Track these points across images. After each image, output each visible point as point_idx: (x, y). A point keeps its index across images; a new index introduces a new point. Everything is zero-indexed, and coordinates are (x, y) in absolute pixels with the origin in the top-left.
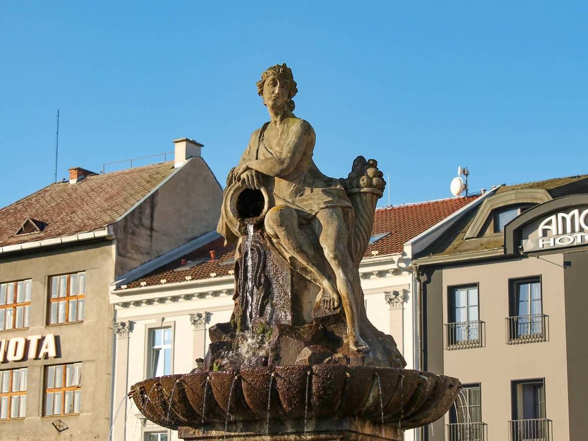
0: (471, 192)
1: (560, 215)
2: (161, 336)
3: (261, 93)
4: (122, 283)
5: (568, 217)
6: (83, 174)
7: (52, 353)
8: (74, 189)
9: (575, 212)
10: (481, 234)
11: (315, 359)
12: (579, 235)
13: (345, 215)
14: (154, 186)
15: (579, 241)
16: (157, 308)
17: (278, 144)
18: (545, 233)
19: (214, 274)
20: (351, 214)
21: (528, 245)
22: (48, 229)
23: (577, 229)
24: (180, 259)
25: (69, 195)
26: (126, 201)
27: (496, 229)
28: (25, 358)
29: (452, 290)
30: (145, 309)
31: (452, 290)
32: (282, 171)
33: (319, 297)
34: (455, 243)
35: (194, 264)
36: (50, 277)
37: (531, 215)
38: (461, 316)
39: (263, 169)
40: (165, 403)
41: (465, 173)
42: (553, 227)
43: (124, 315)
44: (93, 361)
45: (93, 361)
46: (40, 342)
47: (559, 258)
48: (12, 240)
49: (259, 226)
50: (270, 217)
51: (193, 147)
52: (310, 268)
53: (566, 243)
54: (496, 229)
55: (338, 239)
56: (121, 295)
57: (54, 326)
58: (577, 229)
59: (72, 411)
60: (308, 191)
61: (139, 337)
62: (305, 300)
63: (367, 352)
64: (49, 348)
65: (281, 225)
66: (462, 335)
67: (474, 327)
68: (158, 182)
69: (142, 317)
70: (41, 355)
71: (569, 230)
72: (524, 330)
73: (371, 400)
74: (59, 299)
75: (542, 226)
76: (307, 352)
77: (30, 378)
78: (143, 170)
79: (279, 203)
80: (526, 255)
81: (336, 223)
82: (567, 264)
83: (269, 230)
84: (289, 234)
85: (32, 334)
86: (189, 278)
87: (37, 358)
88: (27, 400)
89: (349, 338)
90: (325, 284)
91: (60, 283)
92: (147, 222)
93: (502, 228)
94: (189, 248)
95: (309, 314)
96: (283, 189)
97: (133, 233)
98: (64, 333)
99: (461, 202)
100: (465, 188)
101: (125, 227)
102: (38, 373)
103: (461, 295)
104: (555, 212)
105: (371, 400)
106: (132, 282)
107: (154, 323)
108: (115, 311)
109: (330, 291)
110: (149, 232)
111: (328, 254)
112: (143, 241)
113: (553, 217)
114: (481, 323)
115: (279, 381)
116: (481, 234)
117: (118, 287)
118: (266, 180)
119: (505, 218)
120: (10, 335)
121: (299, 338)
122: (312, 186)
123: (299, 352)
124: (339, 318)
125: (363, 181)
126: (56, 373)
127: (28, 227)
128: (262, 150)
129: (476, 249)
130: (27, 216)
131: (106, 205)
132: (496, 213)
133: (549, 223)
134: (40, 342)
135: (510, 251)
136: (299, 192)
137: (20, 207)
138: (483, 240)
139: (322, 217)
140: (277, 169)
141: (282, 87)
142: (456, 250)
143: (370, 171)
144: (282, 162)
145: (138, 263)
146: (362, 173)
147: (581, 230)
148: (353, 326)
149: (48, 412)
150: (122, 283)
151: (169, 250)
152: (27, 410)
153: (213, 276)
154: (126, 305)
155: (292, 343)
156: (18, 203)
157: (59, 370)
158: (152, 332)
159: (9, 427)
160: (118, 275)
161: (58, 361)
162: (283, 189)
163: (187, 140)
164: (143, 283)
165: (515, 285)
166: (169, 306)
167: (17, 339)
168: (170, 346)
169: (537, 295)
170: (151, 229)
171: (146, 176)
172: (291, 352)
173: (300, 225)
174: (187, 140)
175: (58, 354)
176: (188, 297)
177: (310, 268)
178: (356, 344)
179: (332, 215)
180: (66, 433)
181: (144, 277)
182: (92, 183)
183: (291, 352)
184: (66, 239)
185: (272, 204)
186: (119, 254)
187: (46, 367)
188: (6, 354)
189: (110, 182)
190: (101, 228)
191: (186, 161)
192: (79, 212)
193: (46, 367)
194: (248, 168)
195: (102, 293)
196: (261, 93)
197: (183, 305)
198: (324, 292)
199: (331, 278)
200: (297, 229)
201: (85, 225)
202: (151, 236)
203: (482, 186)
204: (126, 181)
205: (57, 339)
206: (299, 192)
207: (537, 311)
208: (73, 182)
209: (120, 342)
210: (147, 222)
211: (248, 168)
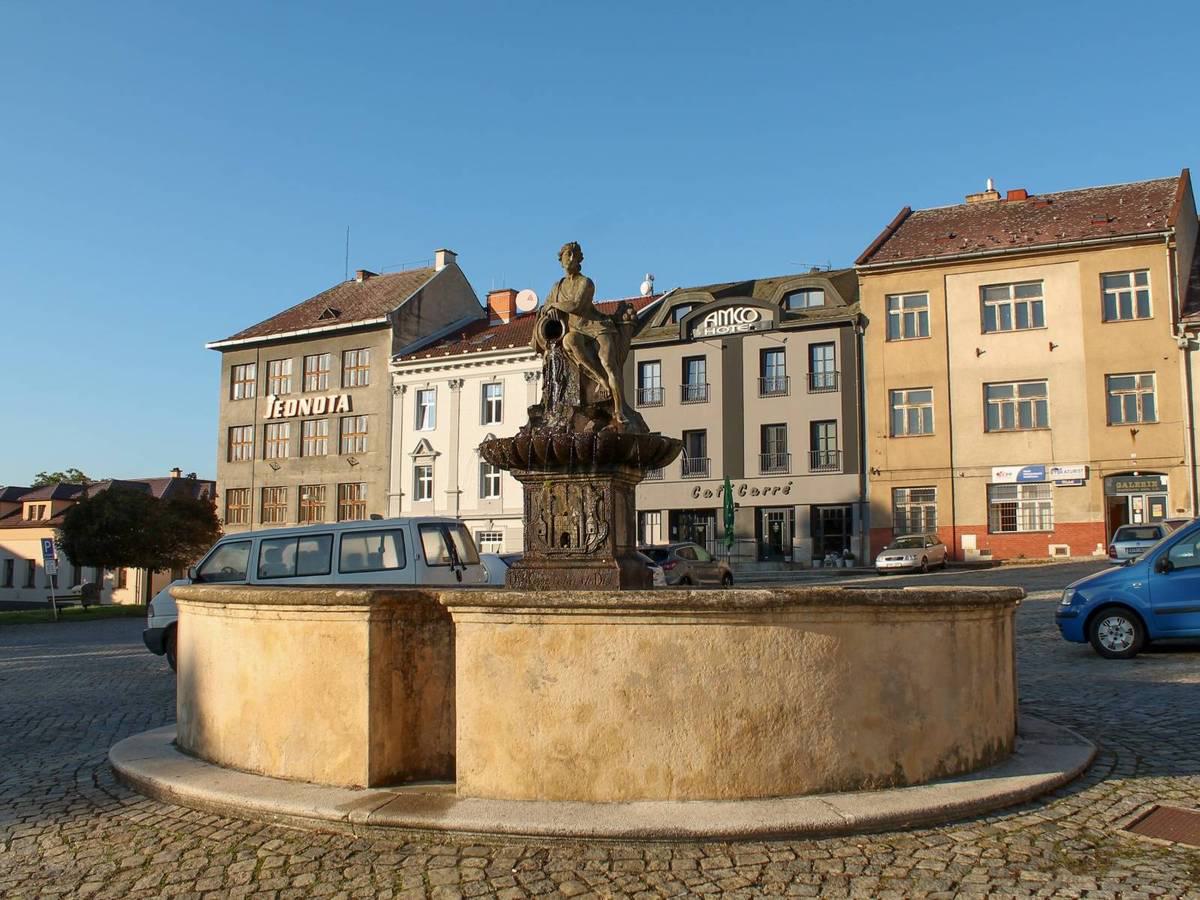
0: (655, 293)
1: (720, 312)
2: (426, 396)
3: (560, 260)
4: (398, 357)
5: (726, 313)
6: (366, 275)
7: (346, 408)
8: (361, 287)
9: (731, 309)
10: (663, 324)
11: (597, 428)
12: (733, 327)
13: (614, 337)
14: (421, 285)
15: (733, 331)
16: (424, 376)
17: (571, 293)
18: (709, 324)
19: (465, 351)
20: (617, 337)
21: (697, 333)
22: (342, 316)
23: (732, 322)
24: (439, 340)
25: (357, 291)
26: (400, 295)
27: (674, 321)
28: (326, 412)
29: (642, 365)
30: (414, 377)
31: (642, 365)
32: (575, 310)
33: (597, 390)
34: (644, 330)
35: (451, 343)
36: (344, 352)
37: (698, 312)
38: (648, 384)
39: (562, 308)
40: (504, 457)
41: (651, 279)
42: (715, 321)
43: (399, 380)
44: (376, 414)
45: (376, 414)
46: (337, 400)
47: (719, 343)
48: (314, 324)
49: (559, 344)
50: (567, 340)
51: (450, 255)
52: (592, 371)
53: (724, 332)
54: (674, 321)
55: (610, 354)
56: (396, 365)
57: (347, 388)
58: (732, 322)
59: (361, 449)
60: (590, 323)
61: (410, 398)
62: (589, 390)
63: (627, 424)
64: (344, 404)
65: (574, 344)
66: (648, 398)
67: (657, 391)
68: (424, 282)
69: (413, 382)
70: (338, 410)
71: (726, 323)
72: (694, 395)
73: (632, 453)
74: (350, 368)
75: (707, 319)
76: (591, 424)
77: (329, 427)
78: (412, 273)
79: (572, 330)
80: (695, 340)
81: (609, 344)
82: (724, 347)
83: (566, 347)
84: (580, 350)
85: (332, 394)
86: (447, 354)
87: (335, 412)
88: (328, 444)
89: (617, 413)
90: (602, 381)
91: (351, 356)
92: (416, 312)
93: (678, 320)
94: (445, 331)
95: (590, 398)
96: (575, 321)
97: (406, 320)
98: (354, 394)
99: (648, 300)
100: (651, 289)
101: (400, 314)
102: (336, 423)
103: (648, 368)
104: (717, 309)
105: (632, 453)
106: (405, 356)
107: (421, 386)
108: (393, 378)
109: (604, 386)
110: (416, 319)
111: (604, 362)
112: (413, 327)
113: (715, 313)
114: (662, 388)
115: (577, 442)
116: (663, 324)
117: (395, 360)
118: (563, 315)
119: (681, 313)
120: (314, 394)
121: (586, 415)
122: (593, 319)
123: (586, 424)
124: (610, 403)
125: (625, 317)
126: (349, 423)
127: (327, 315)
128: (560, 296)
129: (659, 335)
130: (326, 306)
131: (384, 299)
132: (673, 309)
133: (712, 317)
134: (337, 400)
135: (684, 337)
136: (584, 323)
137: (320, 299)
138: (665, 328)
139: (600, 340)
140: (572, 309)
141: (574, 257)
142: (644, 336)
143: (629, 311)
144: (574, 304)
145: (410, 342)
146: (625, 312)
147: (735, 323)
148: (619, 408)
149: (344, 451)
150: (398, 357)
151: (435, 334)
152: (328, 450)
153: (465, 353)
154: (400, 373)
155: (582, 418)
156: (318, 296)
157: (351, 420)
158: (420, 394)
159: (316, 462)
160: (394, 350)
161: (350, 414)
162: (575, 321)
163: (445, 251)
164: (414, 357)
165: (687, 362)
166: (433, 375)
167: (319, 398)
168: (433, 404)
169: (702, 369)
170: (419, 317)
171: (414, 277)
172: (581, 424)
173: (586, 344)
174: (445, 251)
175: (351, 410)
176: (447, 368)
177: (592, 371)
178: (621, 419)
179: (606, 339)
180: (358, 467)
181: (413, 353)
182: (373, 282)
183: (581, 424)
184: (356, 324)
185: (567, 331)
186: (395, 335)
187: (342, 418)
188: (312, 408)
189: (387, 281)
190: (382, 316)
191: (445, 266)
192: (365, 304)
193: (342, 418)
194: (552, 307)
195: (382, 364)
196: (560, 260)
197: (443, 373)
198: (601, 386)
199: (606, 378)
200: (584, 348)
201: (370, 314)
202: (418, 322)
203: (664, 288)
204: (401, 281)
205: (349, 398)
206: (584, 323)
207: (702, 381)
208: (360, 280)
209: (397, 400)
210: (416, 312)
211: (552, 307)
